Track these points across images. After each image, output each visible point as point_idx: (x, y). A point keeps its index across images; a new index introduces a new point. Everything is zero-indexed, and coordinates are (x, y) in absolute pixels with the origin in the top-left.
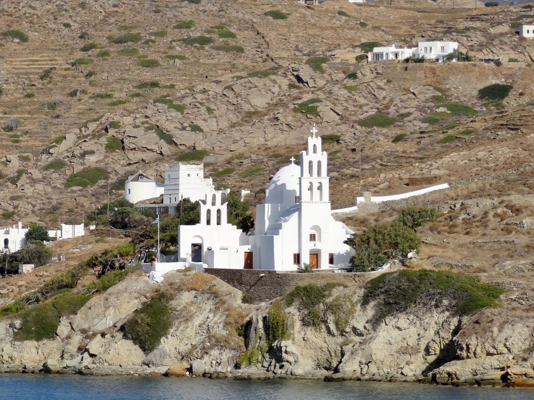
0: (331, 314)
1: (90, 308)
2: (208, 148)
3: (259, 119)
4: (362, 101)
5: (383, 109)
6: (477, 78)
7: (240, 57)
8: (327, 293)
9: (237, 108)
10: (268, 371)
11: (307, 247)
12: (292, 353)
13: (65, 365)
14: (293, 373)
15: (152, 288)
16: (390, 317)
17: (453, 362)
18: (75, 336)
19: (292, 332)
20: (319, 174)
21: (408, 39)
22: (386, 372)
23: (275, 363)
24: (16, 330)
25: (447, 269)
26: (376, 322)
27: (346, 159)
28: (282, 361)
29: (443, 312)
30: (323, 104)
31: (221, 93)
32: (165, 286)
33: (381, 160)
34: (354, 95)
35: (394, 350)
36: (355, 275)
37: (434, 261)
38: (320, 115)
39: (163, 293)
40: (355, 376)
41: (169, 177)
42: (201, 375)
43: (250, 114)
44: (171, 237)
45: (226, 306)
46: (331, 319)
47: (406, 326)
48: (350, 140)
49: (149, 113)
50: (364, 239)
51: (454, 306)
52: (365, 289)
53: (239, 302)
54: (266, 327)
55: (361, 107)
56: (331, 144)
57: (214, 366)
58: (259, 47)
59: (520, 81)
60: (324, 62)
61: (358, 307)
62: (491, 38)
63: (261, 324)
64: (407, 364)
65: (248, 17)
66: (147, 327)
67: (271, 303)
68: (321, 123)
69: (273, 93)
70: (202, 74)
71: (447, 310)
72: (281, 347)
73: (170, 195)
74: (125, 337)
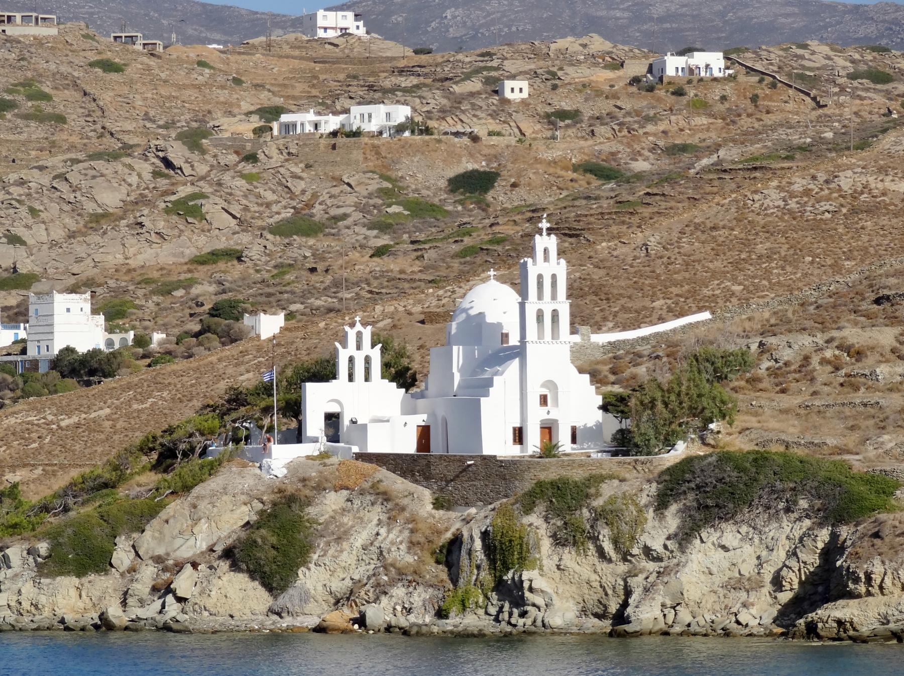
0: (605, 526)
1: (167, 522)
2: (38, 270)
3: (113, 224)
4: (270, 196)
5: (302, 209)
6: (444, 161)
7: (62, 130)
8: (592, 491)
9: (75, 208)
10: (497, 620)
11: (536, 416)
12: (542, 591)
13: (134, 617)
14: (547, 624)
15: (269, 487)
16: (709, 530)
17: (841, 602)
18: (144, 567)
19: (537, 556)
20: (554, 297)
21: (329, 102)
22: (708, 620)
23: (511, 608)
24: (40, 560)
25: (782, 449)
26: (684, 537)
27: (311, 284)
28: (524, 604)
29: (799, 519)
30: (211, 201)
31: (48, 184)
32: (292, 483)
33: (369, 284)
34: (256, 187)
35: (717, 583)
36: (636, 461)
37: (753, 436)
38: (208, 218)
39: (293, 495)
40: (657, 628)
41: (37, 314)
42: (382, 629)
44: (286, 402)
45: (407, 514)
46: (605, 535)
47: (736, 543)
48: (259, 257)
50: (646, 401)
51: (819, 510)
52: (658, 483)
53: (429, 507)
54: (489, 549)
55: (268, 205)
56: (230, 264)
57: (399, 614)
58: (89, 115)
59: (510, 166)
60: (205, 137)
61: (650, 514)
62: (458, 100)
63: (478, 544)
64: (744, 605)
65: (64, 69)
66: (272, 548)
67: (493, 510)
68: (209, 231)
69: (130, 185)
70: (6, 157)
71: (808, 516)
72: (522, 582)
73: (38, 341)
74: (235, 567)
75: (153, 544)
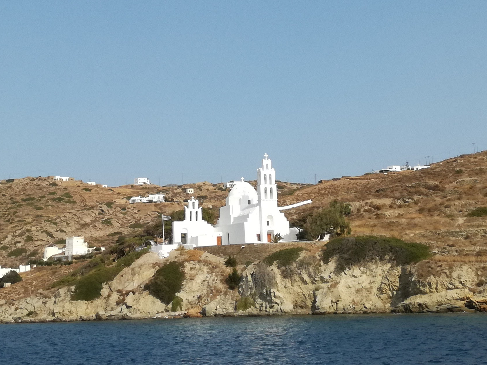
1: (122, 276)
4: (129, 218)
9: (78, 222)
12: (279, 297)
20: (270, 183)
49: (42, 225)
55: (129, 220)
66: (167, 283)
71: (389, 262)
72: (270, 293)
75: (117, 285)
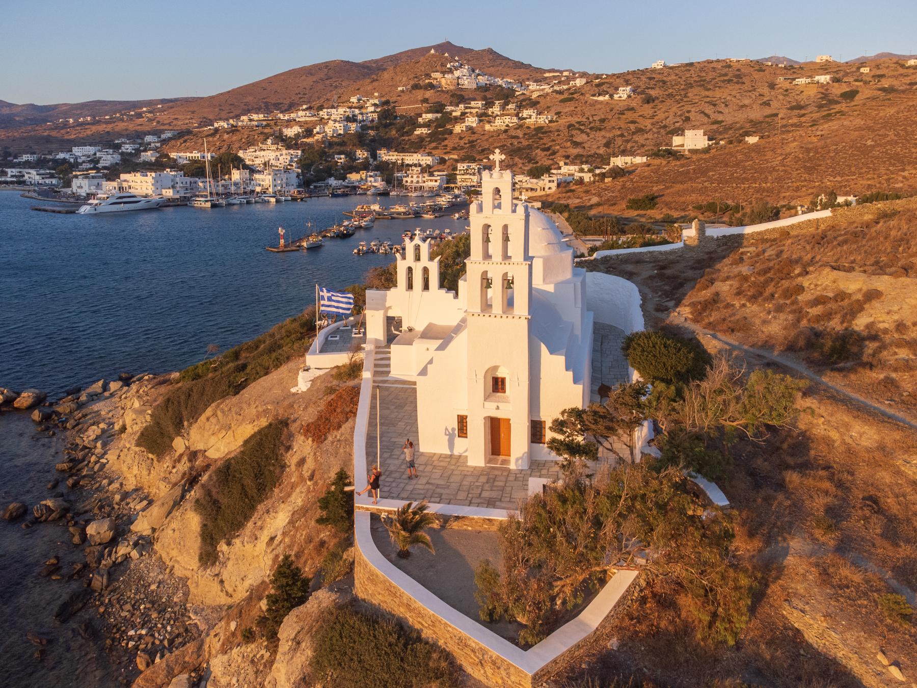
43: (742, 106)
